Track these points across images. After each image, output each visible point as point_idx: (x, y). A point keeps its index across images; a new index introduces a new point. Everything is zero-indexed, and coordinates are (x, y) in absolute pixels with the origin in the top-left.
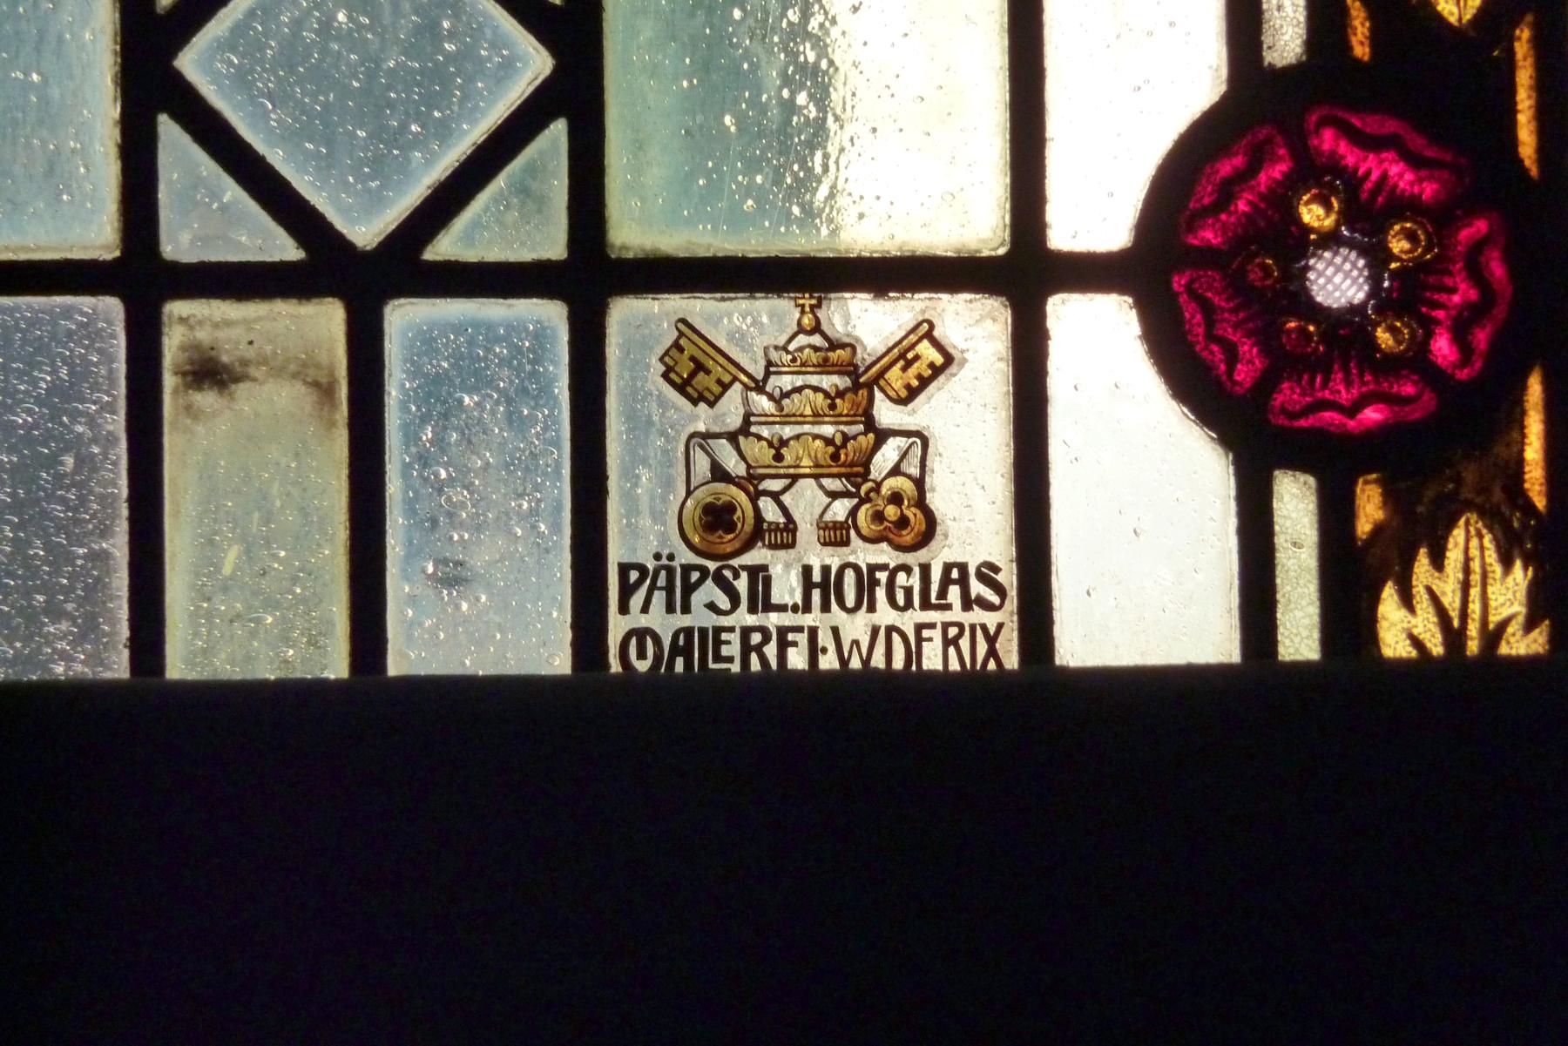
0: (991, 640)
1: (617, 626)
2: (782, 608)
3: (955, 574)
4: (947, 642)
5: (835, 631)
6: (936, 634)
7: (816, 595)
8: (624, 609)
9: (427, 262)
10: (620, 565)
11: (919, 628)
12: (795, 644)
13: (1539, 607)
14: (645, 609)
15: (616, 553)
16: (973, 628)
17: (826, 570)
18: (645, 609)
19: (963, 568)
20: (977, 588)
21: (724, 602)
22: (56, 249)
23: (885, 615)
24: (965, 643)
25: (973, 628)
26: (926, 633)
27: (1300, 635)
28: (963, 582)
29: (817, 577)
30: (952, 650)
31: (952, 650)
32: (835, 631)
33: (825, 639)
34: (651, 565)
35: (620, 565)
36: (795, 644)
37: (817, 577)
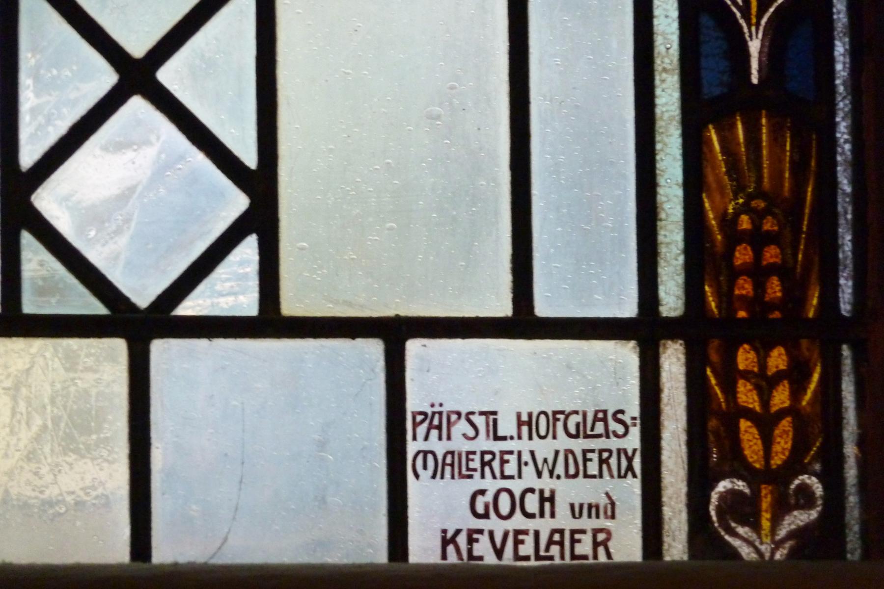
0: (630, 460)
1: (412, 448)
2: (504, 438)
3: (600, 415)
4: (602, 462)
5: (532, 453)
6: (594, 456)
7: (525, 429)
8: (415, 438)
9: (739, 422)
10: (413, 413)
11: (585, 452)
12: (591, 460)
13: (779, 466)
14: (426, 438)
15: (414, 402)
16: (619, 451)
17: (530, 415)
18: (426, 438)
19: (605, 412)
20: (613, 426)
21: (471, 433)
22: (350, 304)
23: (563, 442)
24: (613, 461)
25: (619, 451)
26: (589, 455)
27: (676, 547)
28: (605, 420)
29: (525, 418)
30: (605, 467)
31: (605, 467)
32: (532, 453)
33: (526, 457)
34: (429, 411)
35: (413, 413)
36: (591, 460)
37: (525, 418)
